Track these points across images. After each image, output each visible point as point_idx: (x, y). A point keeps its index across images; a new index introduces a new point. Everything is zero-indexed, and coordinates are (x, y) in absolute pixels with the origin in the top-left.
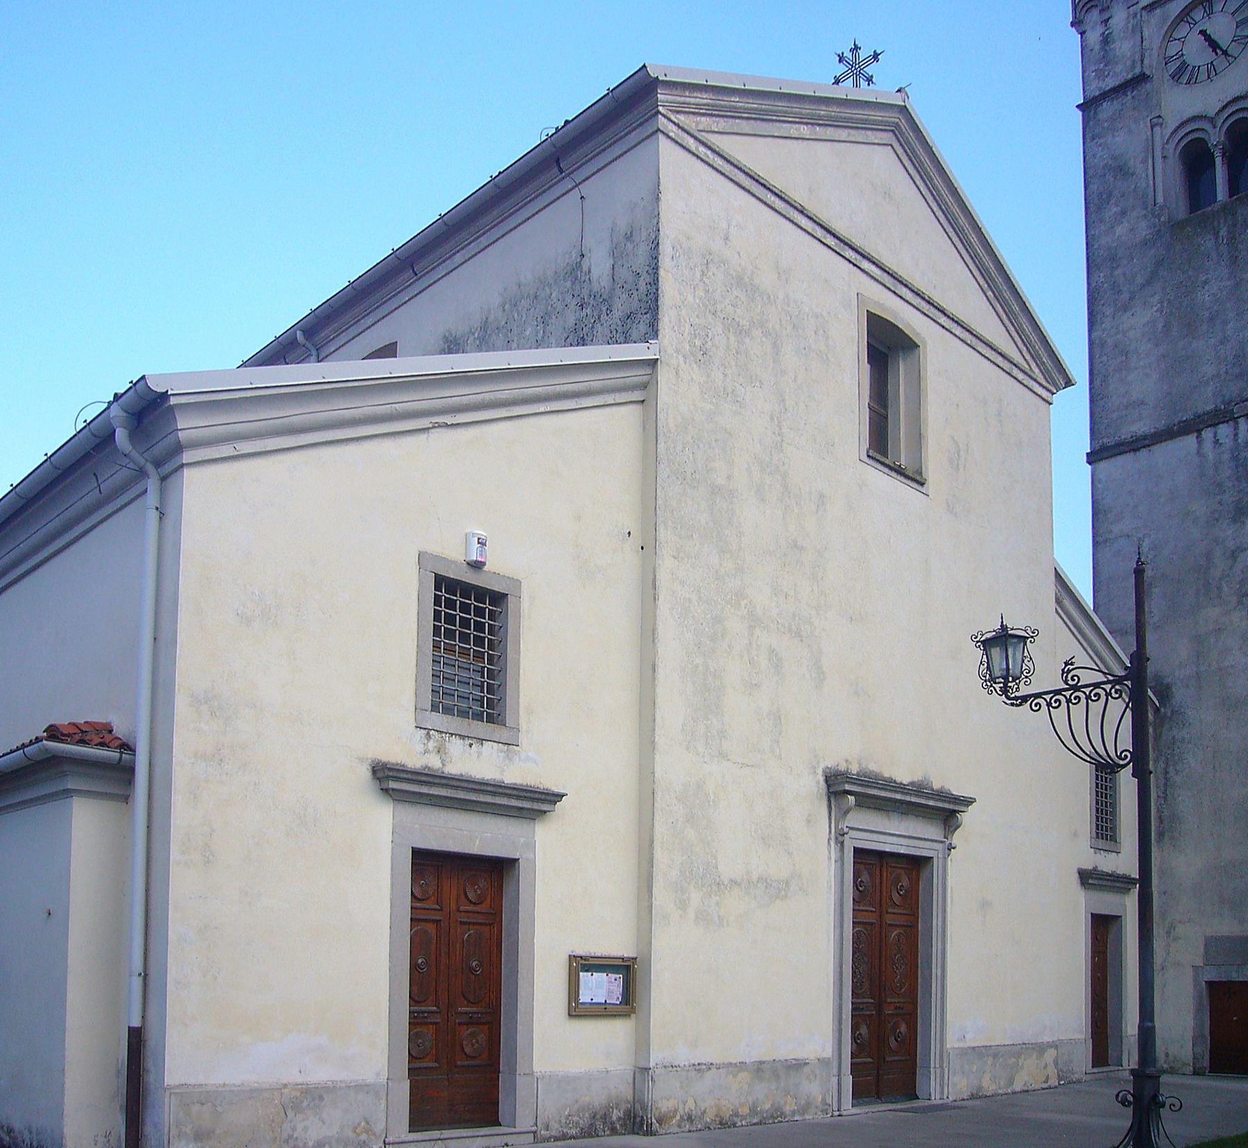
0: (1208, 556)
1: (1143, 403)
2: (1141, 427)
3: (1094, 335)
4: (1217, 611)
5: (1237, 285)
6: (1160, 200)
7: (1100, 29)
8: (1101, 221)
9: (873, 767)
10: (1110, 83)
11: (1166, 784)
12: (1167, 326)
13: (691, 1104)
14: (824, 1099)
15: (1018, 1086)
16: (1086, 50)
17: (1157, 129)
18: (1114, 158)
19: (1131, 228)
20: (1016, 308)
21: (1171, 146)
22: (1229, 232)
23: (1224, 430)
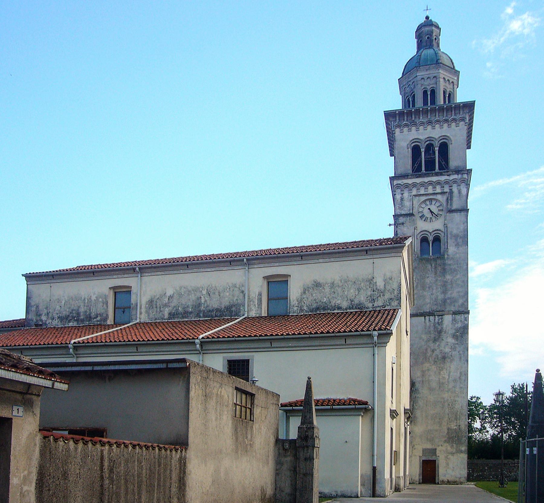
0: (426, 350)
5: (436, 280)
7: (400, 195)
23: (432, 318)
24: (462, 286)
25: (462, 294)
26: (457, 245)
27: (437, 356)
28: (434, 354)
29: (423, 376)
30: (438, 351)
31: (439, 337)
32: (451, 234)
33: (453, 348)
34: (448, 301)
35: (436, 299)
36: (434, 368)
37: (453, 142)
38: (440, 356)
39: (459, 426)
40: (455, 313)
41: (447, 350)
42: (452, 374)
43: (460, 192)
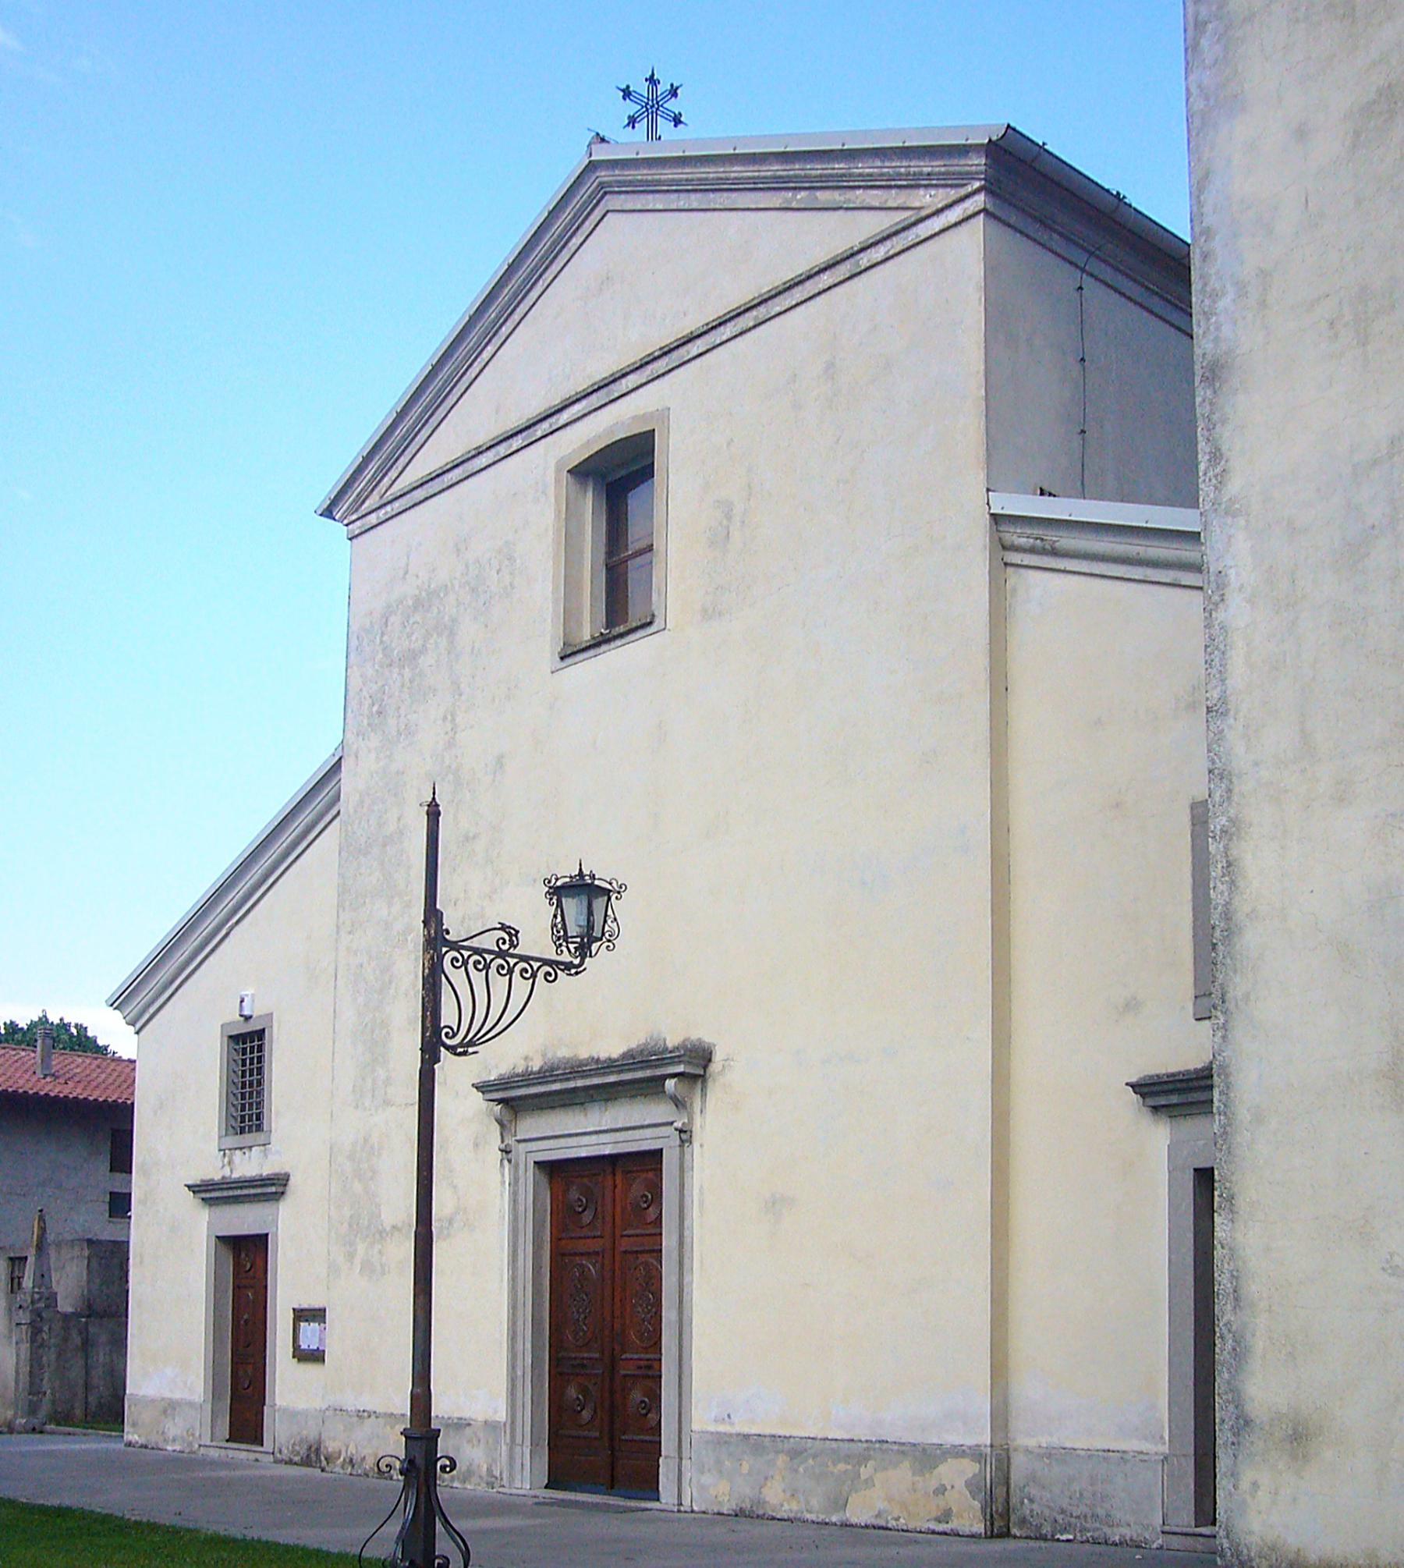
9: (564, 1053)
13: (352, 1449)
14: (489, 1470)
15: (859, 1512)
20: (840, 166)
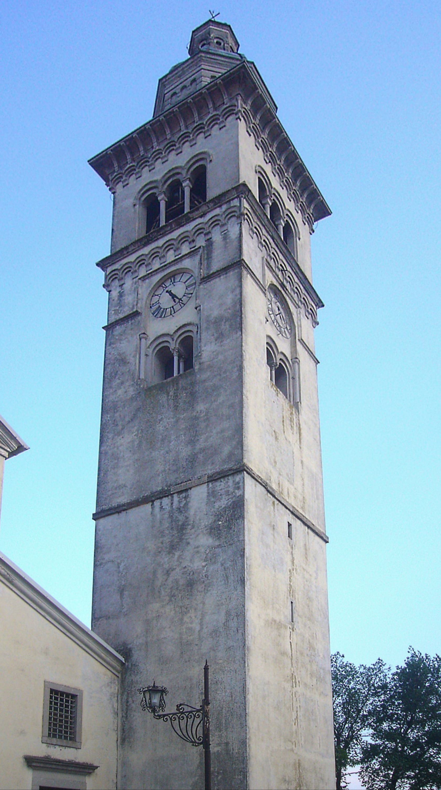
0: (155, 573)
1: (125, 486)
2: (123, 500)
3: (102, 448)
4: (158, 605)
5: (177, 421)
6: (142, 376)
7: (119, 289)
8: (111, 387)
10: (121, 316)
11: (127, 709)
12: (140, 445)
16: (111, 300)
17: (143, 340)
18: (120, 354)
19: (126, 391)
21: (151, 350)
22: (174, 393)
23: (166, 501)
24: (229, 417)
25: (228, 434)
26: (220, 337)
27: (177, 581)
28: (170, 579)
29: (147, 631)
30: (178, 570)
31: (181, 539)
32: (207, 321)
33: (211, 559)
34: (200, 456)
35: (176, 460)
36: (169, 610)
37: (214, 158)
38: (182, 582)
39: (227, 744)
40: (213, 479)
41: (198, 564)
42: (207, 618)
43: (225, 237)
